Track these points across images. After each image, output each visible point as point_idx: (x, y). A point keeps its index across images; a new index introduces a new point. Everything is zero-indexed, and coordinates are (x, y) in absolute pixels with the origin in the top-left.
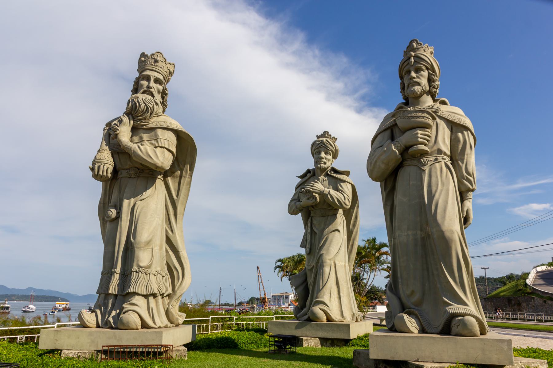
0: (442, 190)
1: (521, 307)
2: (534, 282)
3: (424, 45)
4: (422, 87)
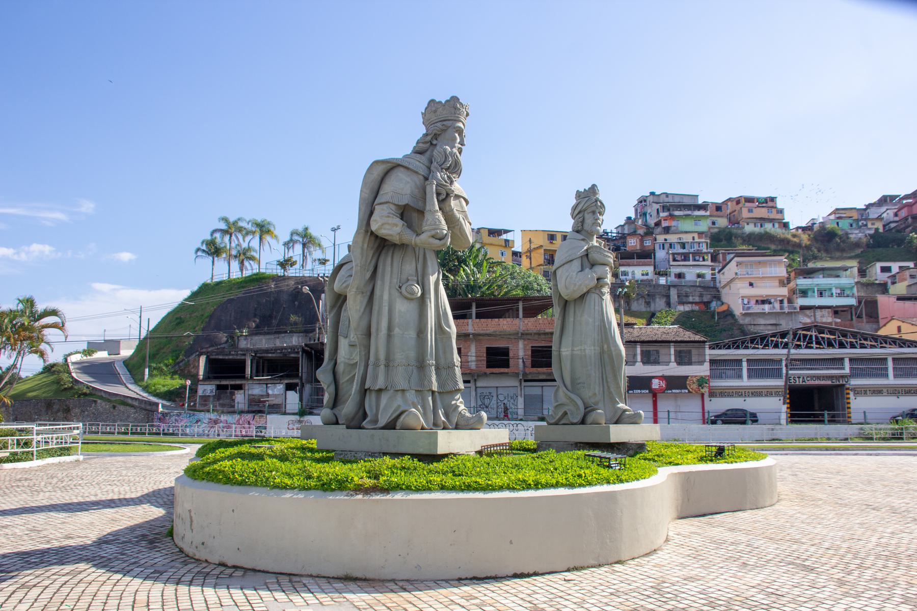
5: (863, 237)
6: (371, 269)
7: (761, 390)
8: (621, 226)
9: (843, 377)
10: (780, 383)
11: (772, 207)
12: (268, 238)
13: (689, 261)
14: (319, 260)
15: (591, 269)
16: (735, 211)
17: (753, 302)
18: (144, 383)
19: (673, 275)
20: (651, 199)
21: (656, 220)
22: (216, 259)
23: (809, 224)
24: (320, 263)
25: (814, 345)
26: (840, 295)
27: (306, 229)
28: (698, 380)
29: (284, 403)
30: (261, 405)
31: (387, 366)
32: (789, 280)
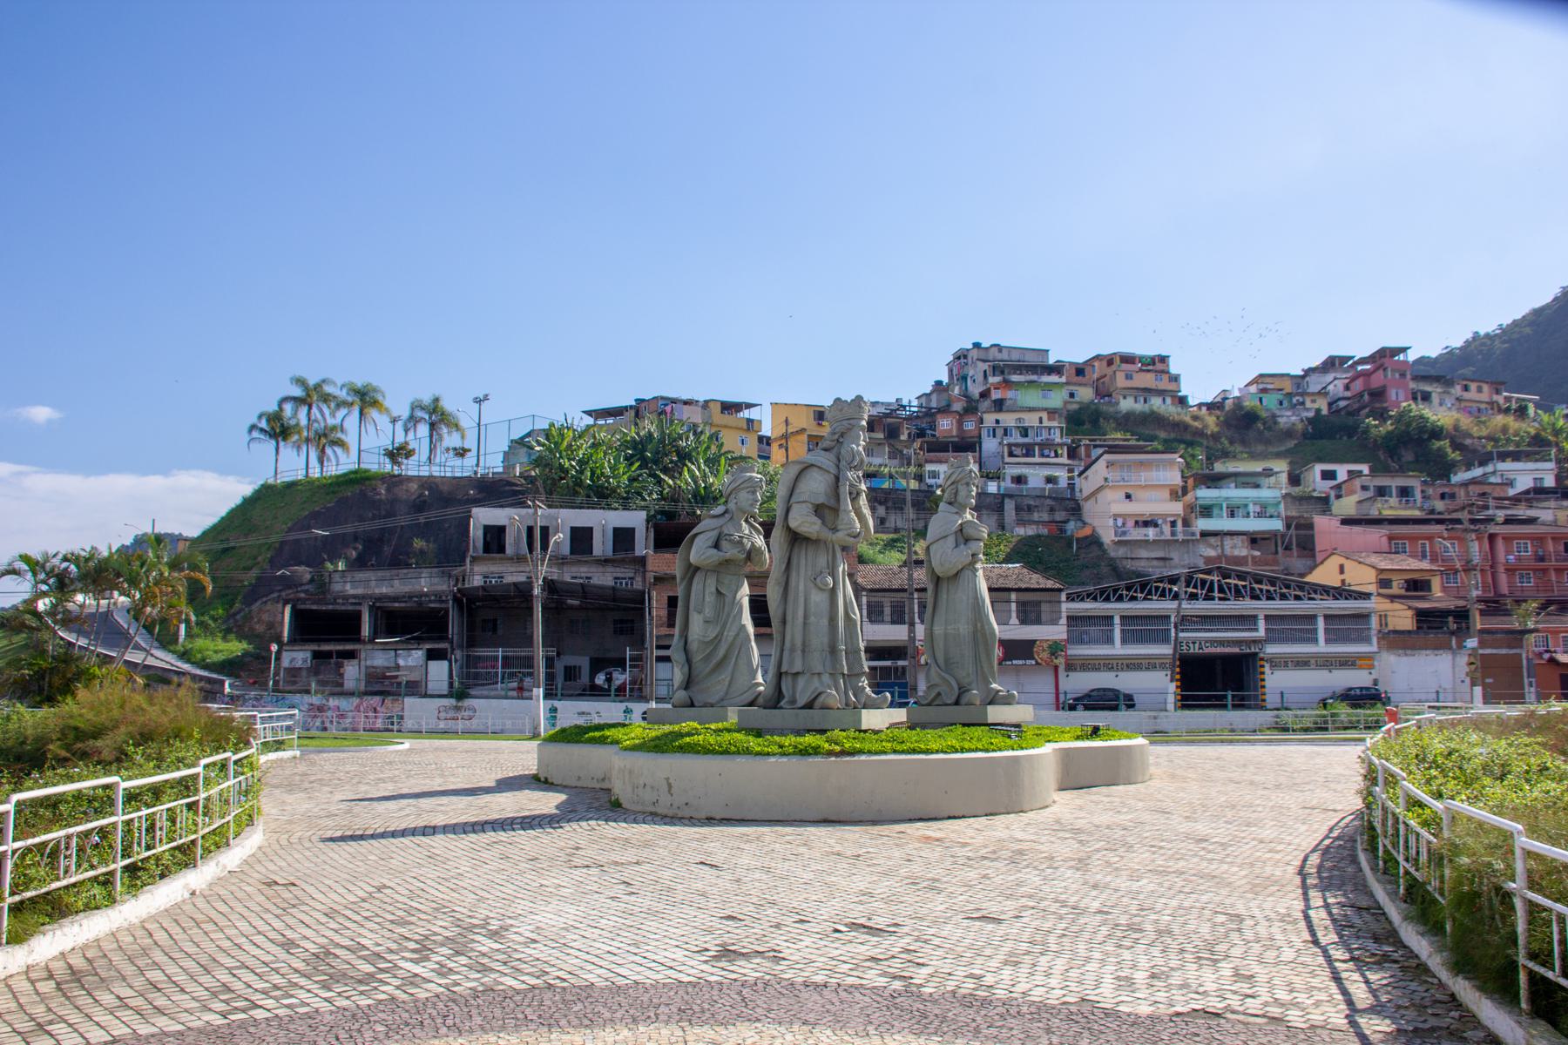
5: (1297, 422)
6: (786, 561)
7: (1139, 661)
8: (924, 394)
9: (1255, 642)
10: (1166, 650)
11: (1163, 372)
12: (373, 413)
13: (1034, 456)
14: (455, 449)
15: (965, 544)
16: (1105, 376)
17: (1131, 523)
18: (180, 648)
19: (1008, 479)
20: (975, 354)
21: (982, 389)
22: (282, 444)
23: (1219, 399)
24: (456, 454)
25: (1216, 594)
26: (1260, 515)
27: (437, 400)
28: (1050, 647)
29: (424, 679)
30: (387, 682)
31: (803, 651)
32: (1185, 491)
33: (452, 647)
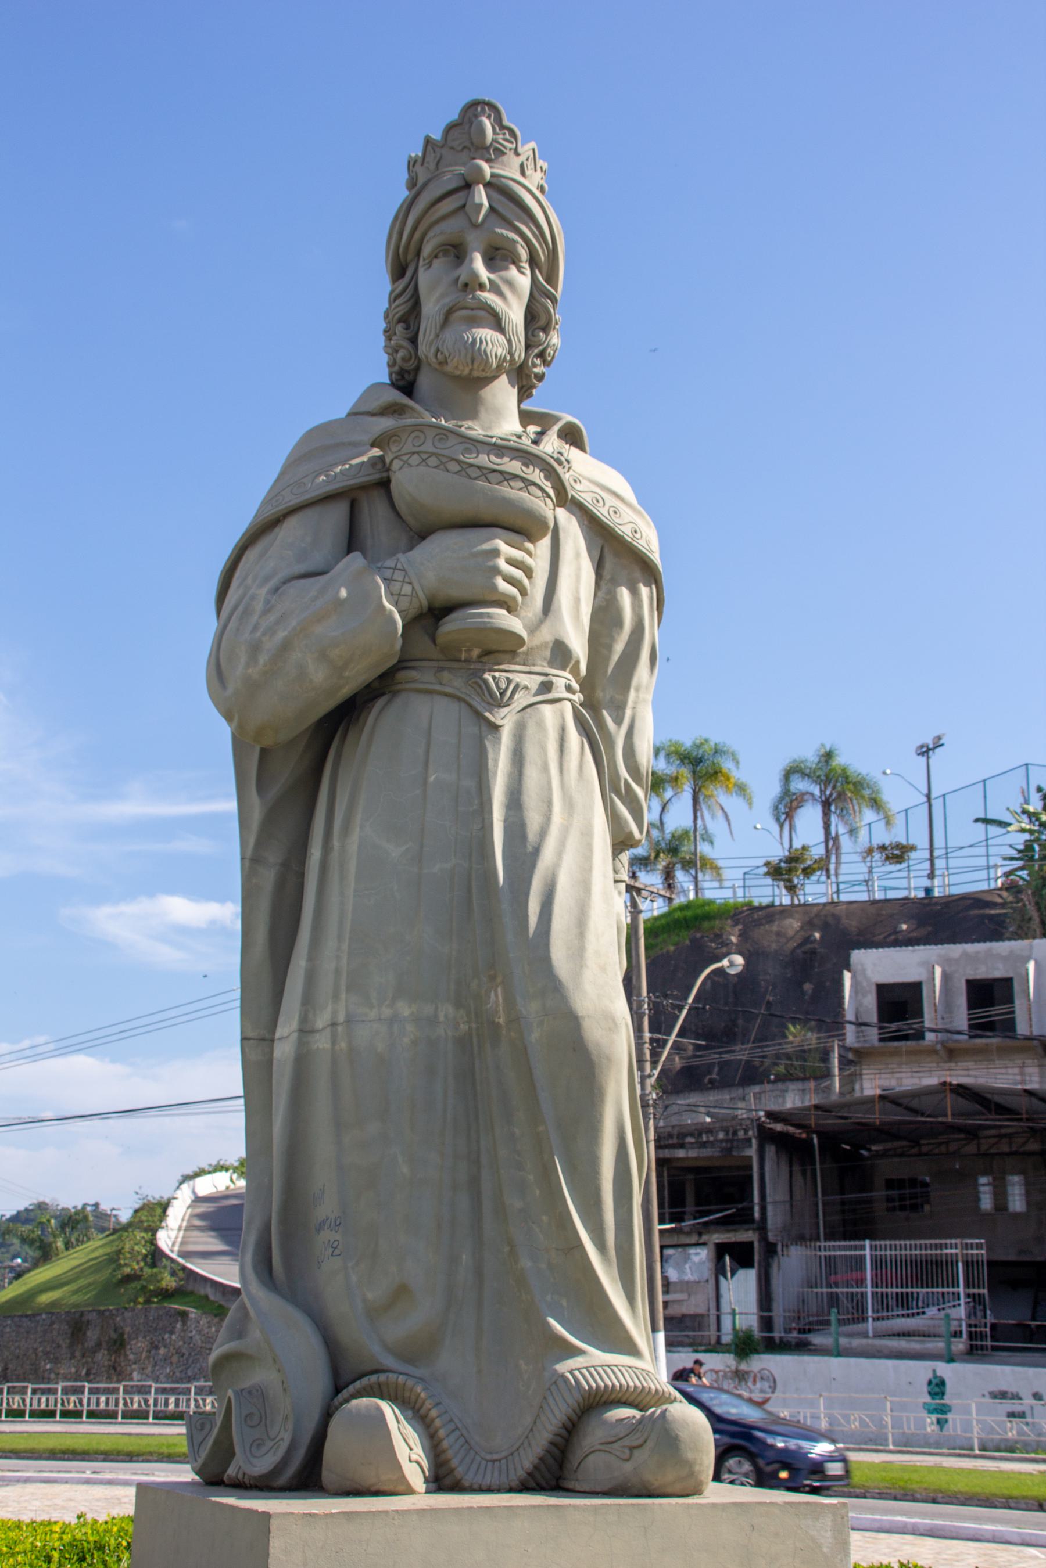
0: (565, 831)
1: (126, 1356)
2: (182, 1243)
3: (523, 145)
4: (509, 341)
14: (883, 848)
24: (887, 858)
27: (828, 756)
29: (713, 1311)
33: (764, 1238)
